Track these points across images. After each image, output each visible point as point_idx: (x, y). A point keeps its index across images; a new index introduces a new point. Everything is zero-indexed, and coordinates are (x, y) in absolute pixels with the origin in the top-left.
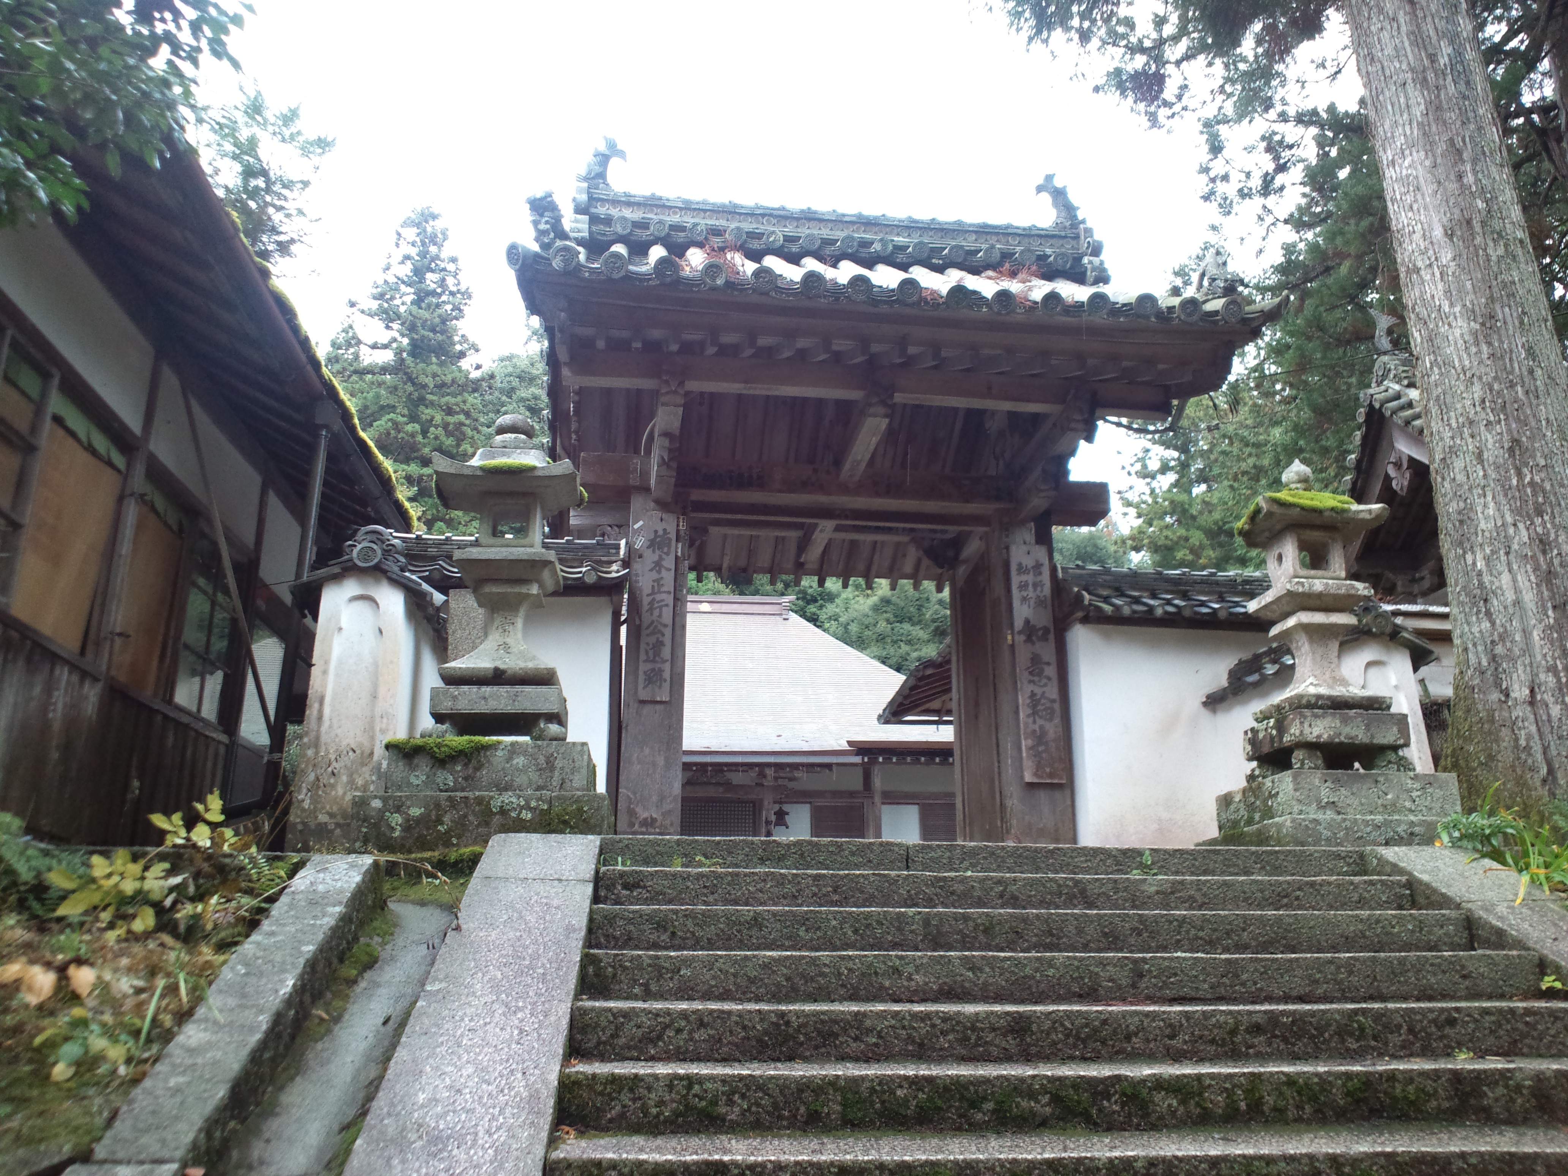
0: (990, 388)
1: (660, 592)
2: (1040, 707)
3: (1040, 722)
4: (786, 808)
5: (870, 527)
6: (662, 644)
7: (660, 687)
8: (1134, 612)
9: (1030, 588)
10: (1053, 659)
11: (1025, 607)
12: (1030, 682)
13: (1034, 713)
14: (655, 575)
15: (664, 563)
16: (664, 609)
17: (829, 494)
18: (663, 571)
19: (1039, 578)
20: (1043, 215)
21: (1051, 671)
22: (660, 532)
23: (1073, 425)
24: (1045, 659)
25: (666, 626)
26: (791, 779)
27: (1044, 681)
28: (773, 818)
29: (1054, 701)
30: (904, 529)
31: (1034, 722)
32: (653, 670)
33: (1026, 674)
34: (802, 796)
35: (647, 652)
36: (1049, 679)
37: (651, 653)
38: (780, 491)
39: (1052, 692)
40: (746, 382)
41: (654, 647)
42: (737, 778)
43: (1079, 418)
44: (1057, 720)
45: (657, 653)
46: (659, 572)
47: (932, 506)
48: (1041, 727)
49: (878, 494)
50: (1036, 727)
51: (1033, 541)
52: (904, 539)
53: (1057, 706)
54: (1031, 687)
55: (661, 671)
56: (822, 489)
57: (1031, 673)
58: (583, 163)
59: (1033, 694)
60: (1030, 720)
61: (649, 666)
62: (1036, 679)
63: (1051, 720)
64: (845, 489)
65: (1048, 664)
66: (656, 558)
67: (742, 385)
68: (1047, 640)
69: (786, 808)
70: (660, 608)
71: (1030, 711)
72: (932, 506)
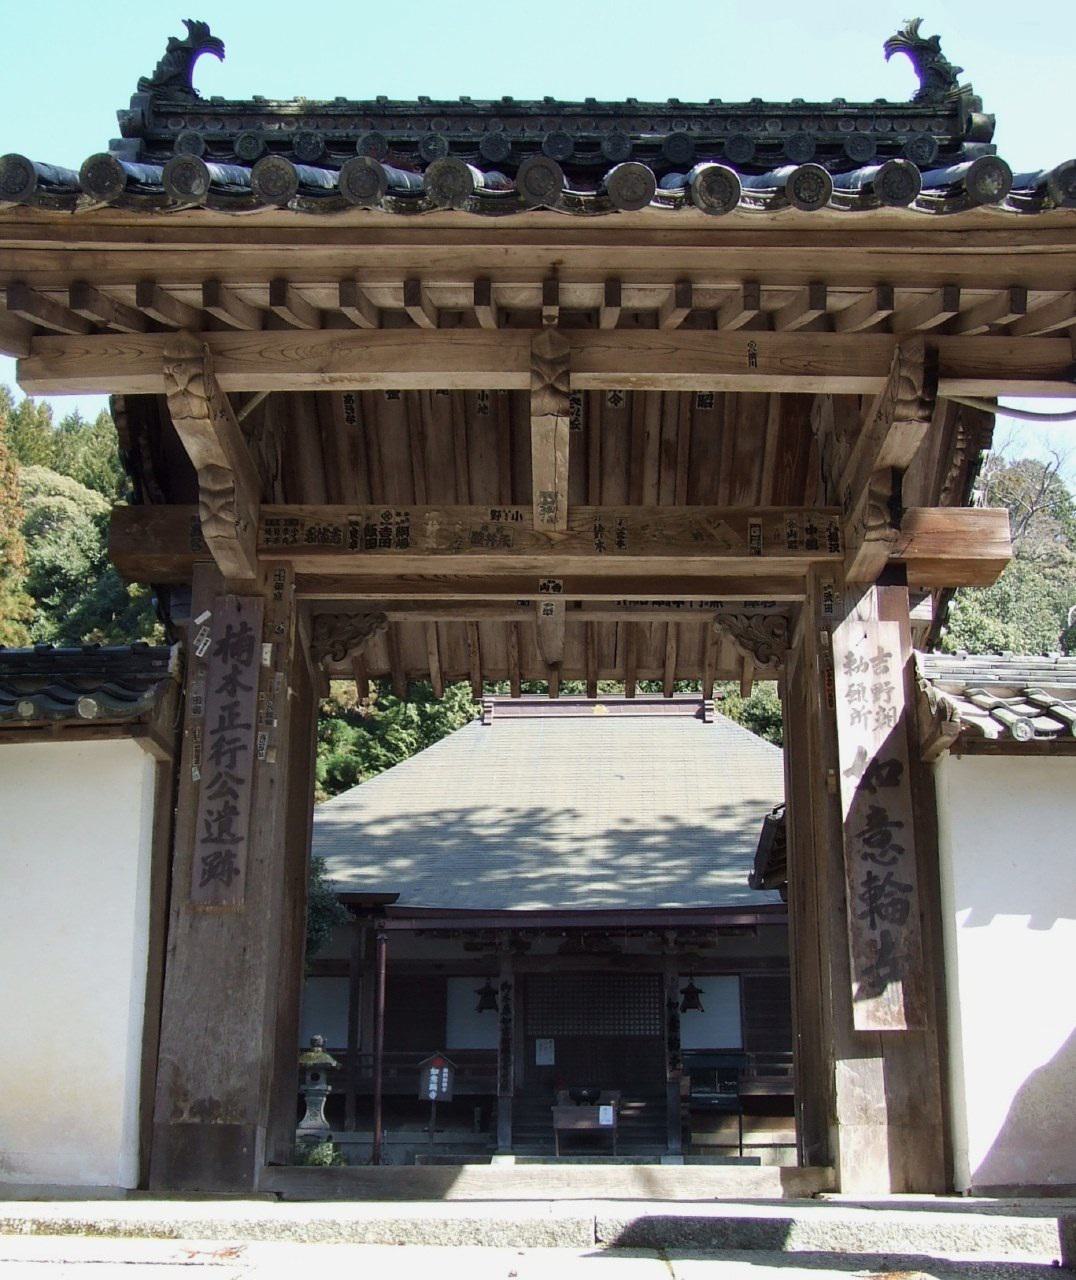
0: (753, 356)
1: (233, 727)
2: (883, 900)
3: (883, 925)
4: (698, 982)
5: (668, 603)
6: (234, 811)
7: (228, 884)
8: (1039, 733)
9: (869, 695)
10: (907, 818)
11: (859, 726)
12: (865, 857)
13: (873, 911)
14: (224, 699)
15: (242, 679)
16: (240, 754)
17: (519, 552)
18: (240, 693)
19: (883, 678)
20: (900, 83)
21: (903, 837)
22: (237, 629)
23: (901, 411)
24: (892, 817)
25: (240, 781)
26: (703, 945)
27: (892, 854)
28: (681, 998)
29: (908, 888)
30: (702, 604)
31: (873, 925)
32: (218, 855)
33: (859, 844)
34: (722, 967)
35: (208, 826)
36: (901, 851)
37: (215, 829)
38: (434, 552)
39: (906, 872)
40: (321, 370)
41: (220, 816)
42: (627, 945)
43: (909, 397)
44: (914, 921)
45: (225, 827)
46: (232, 693)
47: (698, 564)
48: (885, 934)
49: (601, 548)
50: (876, 935)
51: (875, 615)
52: (708, 617)
53: (913, 899)
54: (869, 865)
55: (231, 855)
56: (499, 541)
57: (867, 842)
58: (148, 61)
59: (871, 878)
60: (866, 923)
61: (212, 848)
62: (877, 851)
63: (902, 921)
64: (545, 543)
65: (899, 825)
66: (228, 670)
67: (317, 376)
68: (897, 783)
69: (698, 982)
70: (233, 752)
71: (863, 907)
72: (698, 564)
